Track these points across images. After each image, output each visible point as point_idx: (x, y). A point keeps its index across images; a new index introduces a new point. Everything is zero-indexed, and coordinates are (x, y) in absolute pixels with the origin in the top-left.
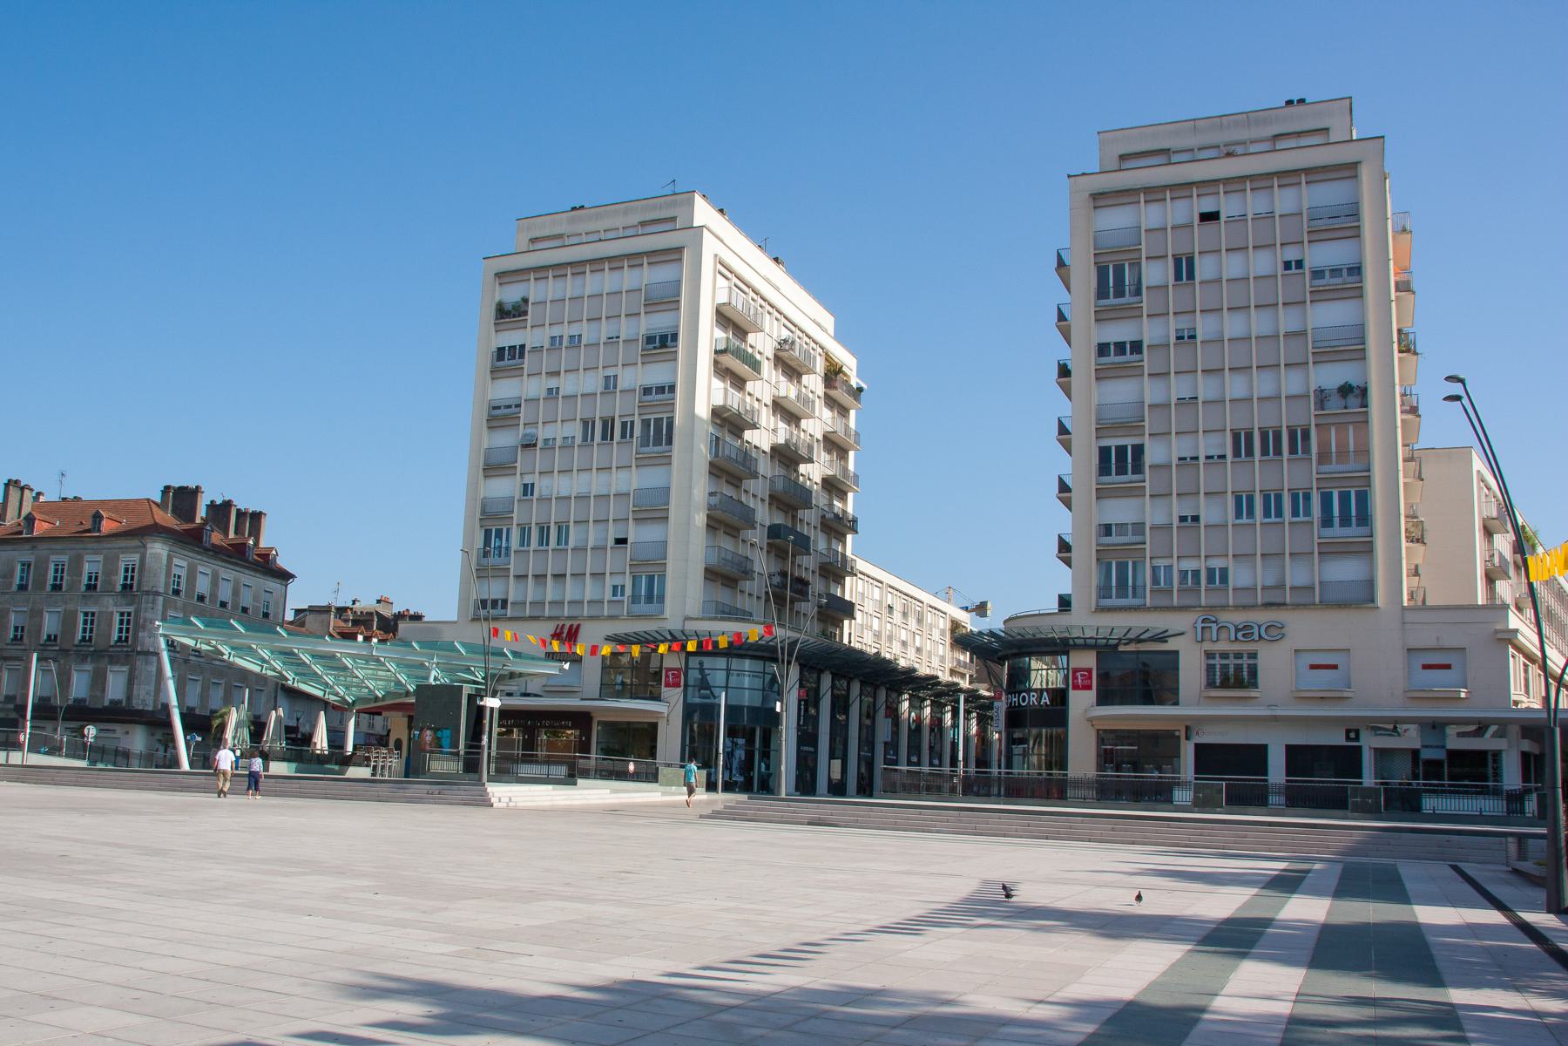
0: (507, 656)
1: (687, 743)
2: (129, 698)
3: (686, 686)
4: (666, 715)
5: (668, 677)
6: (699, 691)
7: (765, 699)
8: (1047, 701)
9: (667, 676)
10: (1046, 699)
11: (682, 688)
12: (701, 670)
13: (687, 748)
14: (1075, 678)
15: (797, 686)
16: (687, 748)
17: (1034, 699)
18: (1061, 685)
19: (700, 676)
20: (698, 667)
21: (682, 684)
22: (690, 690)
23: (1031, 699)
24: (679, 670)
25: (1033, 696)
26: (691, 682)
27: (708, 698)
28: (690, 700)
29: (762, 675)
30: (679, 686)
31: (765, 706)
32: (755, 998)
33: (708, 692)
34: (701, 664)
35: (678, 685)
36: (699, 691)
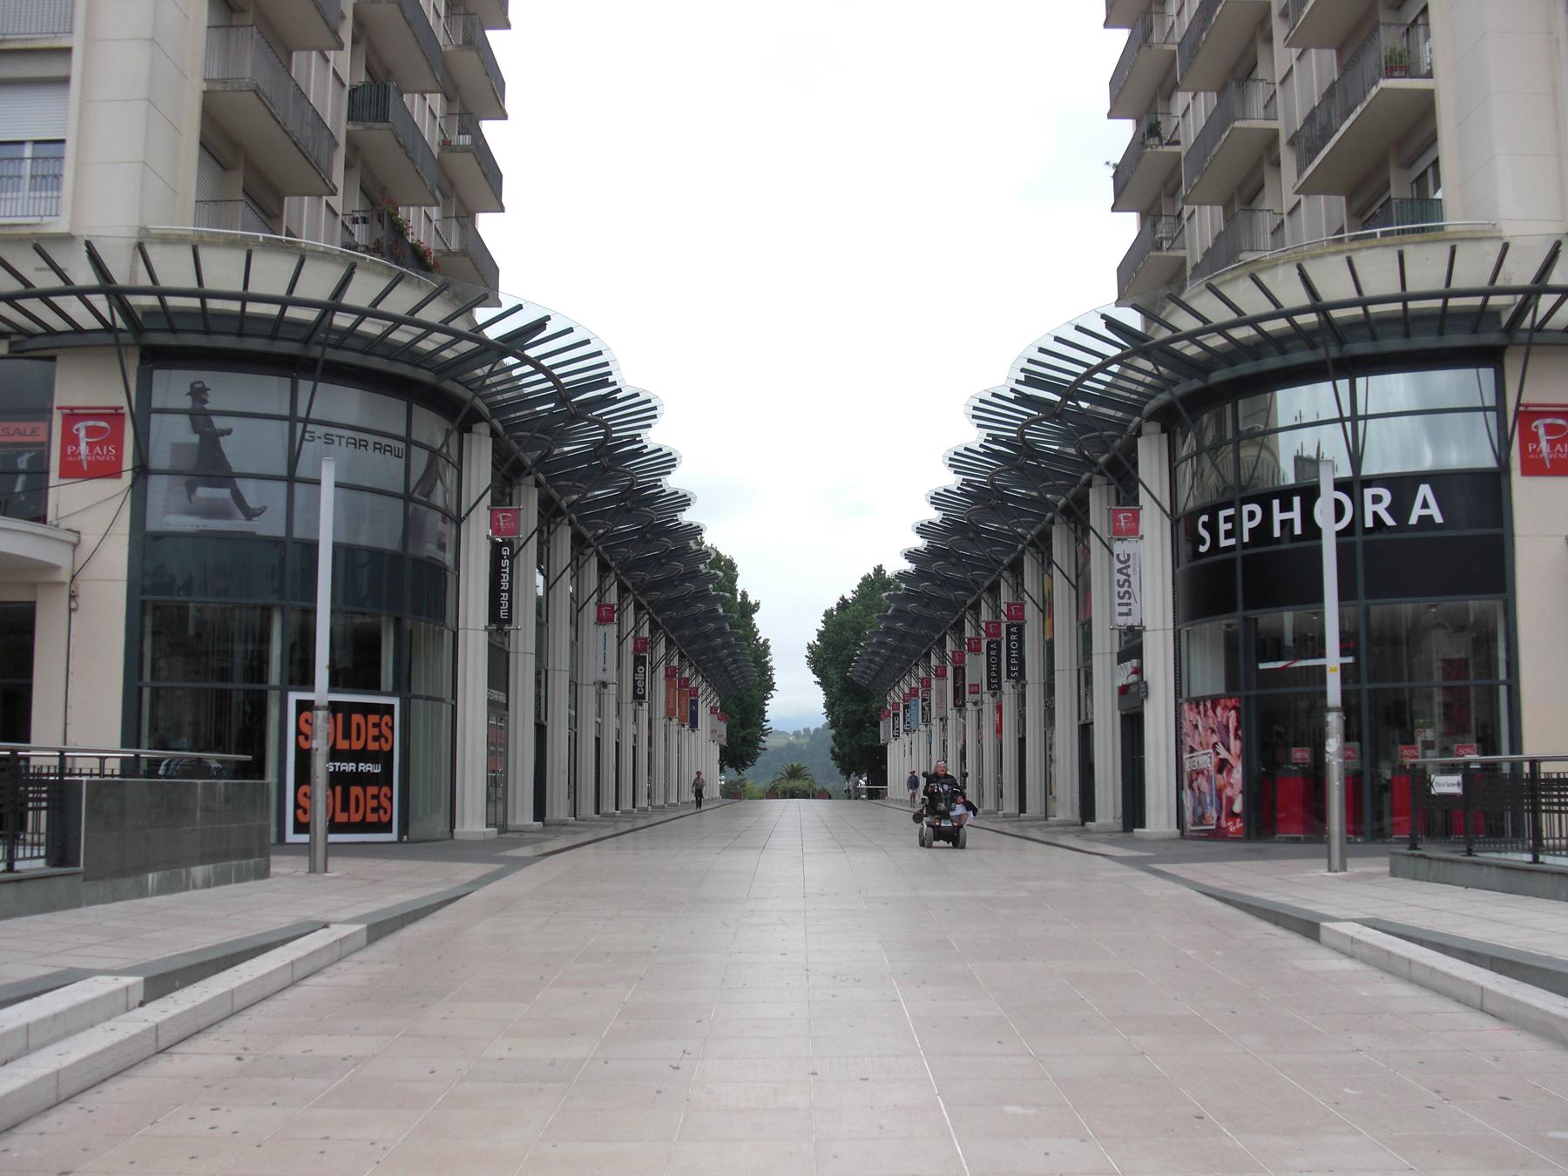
0: (1049, 1079)
1: (1503, 690)
2: (419, 697)
3: (142, 471)
4: (65, 576)
5: (75, 441)
6: (191, 489)
7: (411, 528)
8: (1434, 511)
9: (69, 439)
10: (1426, 505)
11: (127, 478)
12: (200, 416)
13: (1502, 675)
14: (1529, 437)
15: (487, 500)
16: (1502, 675)
17: (1381, 509)
18: (1488, 461)
19: (196, 439)
20: (187, 403)
21: (128, 462)
22: (158, 487)
23: (1369, 508)
24: (114, 416)
25: (1377, 499)
26: (160, 457)
27: (225, 514)
28: (154, 524)
29: (402, 445)
30: (117, 474)
31: (411, 551)
32: (27, 354)
33: (225, 493)
34: (198, 393)
35: (111, 471)
36: (191, 489)
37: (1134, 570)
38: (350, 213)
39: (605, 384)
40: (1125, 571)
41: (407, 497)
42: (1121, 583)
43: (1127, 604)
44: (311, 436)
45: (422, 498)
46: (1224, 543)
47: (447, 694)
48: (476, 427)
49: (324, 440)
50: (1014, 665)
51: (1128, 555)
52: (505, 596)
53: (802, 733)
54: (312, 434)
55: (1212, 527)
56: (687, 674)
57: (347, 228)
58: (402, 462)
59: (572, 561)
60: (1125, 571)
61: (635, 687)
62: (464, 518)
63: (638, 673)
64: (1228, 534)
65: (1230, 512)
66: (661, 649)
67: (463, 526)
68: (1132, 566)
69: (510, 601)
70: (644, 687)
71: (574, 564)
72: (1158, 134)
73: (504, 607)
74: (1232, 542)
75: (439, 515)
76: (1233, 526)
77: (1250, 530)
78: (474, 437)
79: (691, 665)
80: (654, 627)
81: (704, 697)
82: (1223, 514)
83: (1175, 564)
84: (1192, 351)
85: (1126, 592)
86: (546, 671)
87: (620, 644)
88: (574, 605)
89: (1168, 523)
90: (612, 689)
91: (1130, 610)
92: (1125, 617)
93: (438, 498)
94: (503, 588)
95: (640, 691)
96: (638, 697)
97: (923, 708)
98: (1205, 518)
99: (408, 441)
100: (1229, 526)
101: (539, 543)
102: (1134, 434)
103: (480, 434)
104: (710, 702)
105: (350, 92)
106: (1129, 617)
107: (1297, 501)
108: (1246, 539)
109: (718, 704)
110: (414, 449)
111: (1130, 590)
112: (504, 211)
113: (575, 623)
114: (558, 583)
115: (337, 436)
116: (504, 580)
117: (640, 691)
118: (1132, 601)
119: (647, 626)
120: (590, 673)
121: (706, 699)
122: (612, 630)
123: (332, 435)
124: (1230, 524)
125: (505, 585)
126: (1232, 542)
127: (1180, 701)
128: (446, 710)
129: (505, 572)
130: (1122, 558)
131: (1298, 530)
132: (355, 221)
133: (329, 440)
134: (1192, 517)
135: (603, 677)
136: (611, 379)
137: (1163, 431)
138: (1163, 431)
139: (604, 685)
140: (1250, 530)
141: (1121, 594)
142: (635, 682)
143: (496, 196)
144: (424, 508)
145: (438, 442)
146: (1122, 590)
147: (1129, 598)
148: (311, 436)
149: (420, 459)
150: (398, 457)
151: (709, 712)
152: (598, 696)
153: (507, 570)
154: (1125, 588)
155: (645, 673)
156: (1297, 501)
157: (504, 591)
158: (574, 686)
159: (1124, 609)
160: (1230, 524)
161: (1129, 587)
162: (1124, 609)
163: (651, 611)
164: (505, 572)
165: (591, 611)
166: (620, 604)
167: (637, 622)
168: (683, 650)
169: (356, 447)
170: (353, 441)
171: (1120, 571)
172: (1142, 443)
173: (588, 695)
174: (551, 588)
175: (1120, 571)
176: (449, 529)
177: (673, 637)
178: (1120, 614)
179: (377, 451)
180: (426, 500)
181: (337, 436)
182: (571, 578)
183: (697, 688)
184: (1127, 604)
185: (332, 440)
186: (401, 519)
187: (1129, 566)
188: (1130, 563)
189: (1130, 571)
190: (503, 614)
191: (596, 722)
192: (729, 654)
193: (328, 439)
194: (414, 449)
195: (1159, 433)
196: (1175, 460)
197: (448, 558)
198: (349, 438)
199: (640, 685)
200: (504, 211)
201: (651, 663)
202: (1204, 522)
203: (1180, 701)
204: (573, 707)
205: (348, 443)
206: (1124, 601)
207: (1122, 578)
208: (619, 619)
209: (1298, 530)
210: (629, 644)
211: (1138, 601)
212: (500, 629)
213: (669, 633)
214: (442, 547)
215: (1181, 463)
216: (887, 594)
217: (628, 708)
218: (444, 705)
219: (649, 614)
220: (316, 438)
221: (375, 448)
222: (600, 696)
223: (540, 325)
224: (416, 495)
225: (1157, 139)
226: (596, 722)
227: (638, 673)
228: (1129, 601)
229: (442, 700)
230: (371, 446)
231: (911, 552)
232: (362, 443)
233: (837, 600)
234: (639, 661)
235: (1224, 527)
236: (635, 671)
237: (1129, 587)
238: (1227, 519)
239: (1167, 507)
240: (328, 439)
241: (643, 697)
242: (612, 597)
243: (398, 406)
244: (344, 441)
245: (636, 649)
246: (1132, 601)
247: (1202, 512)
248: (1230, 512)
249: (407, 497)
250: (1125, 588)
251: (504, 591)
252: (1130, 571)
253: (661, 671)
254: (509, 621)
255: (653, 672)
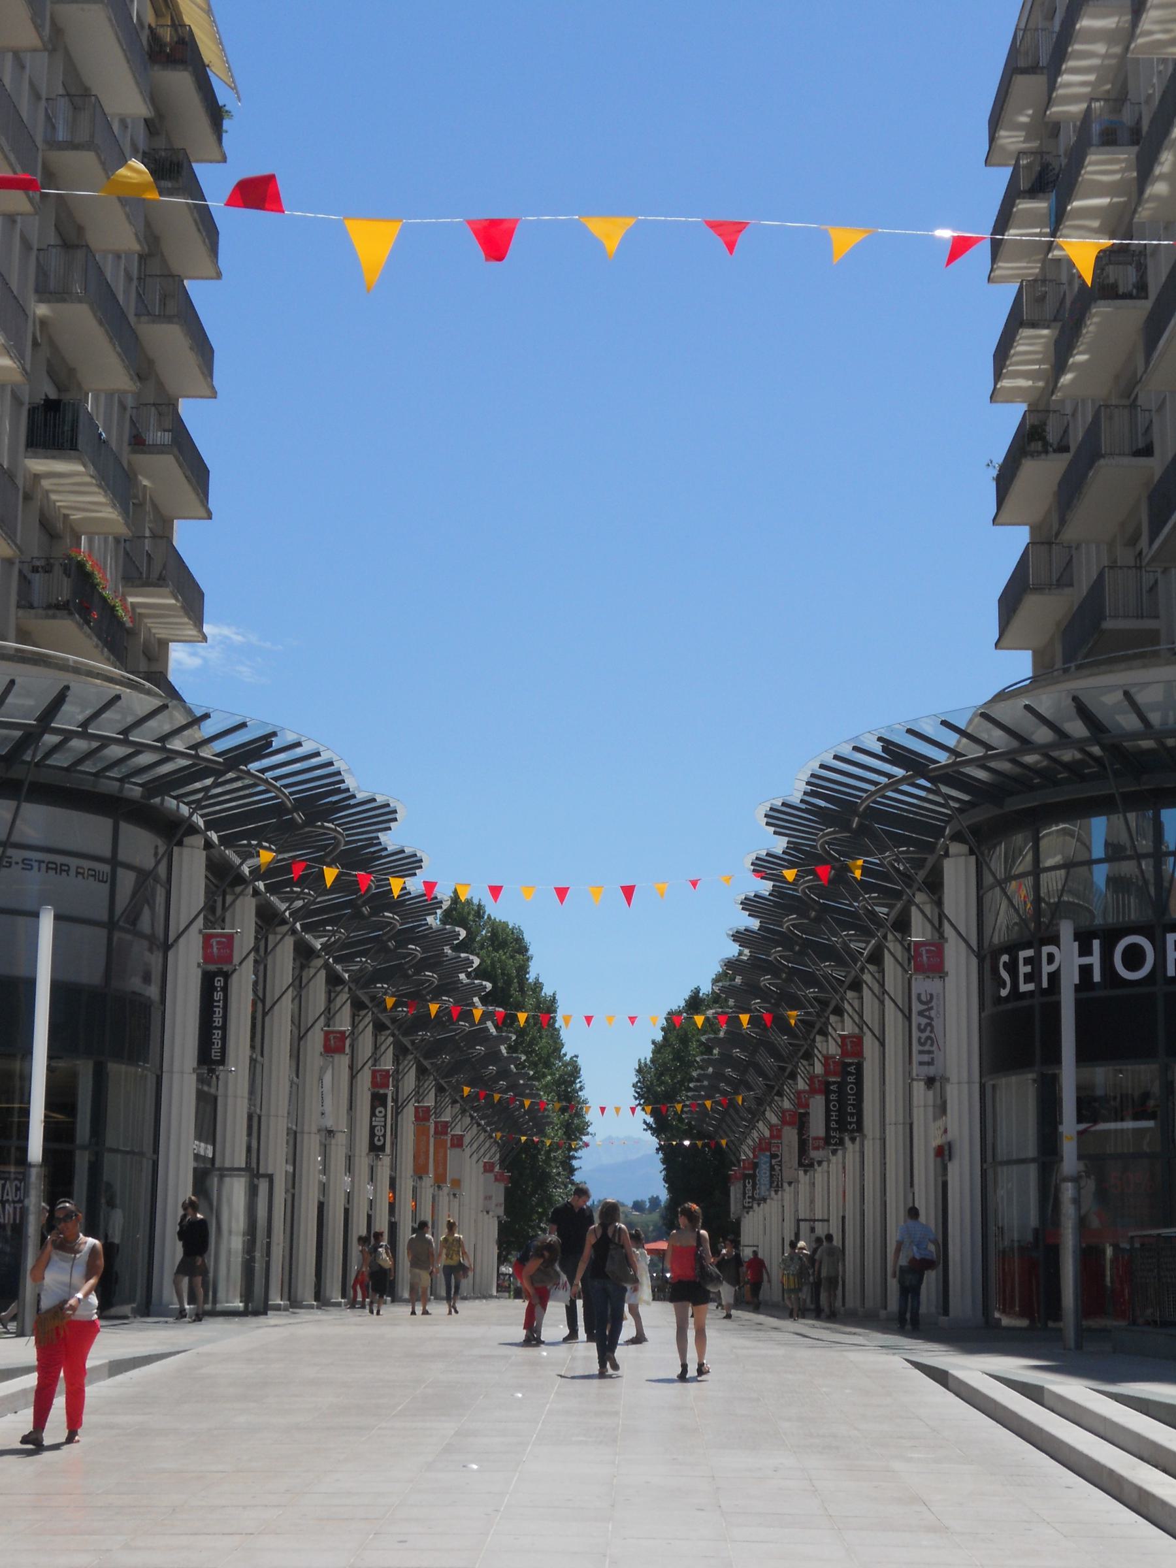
37: (938, 1012)
38: (29, 560)
39: (339, 791)
40: (927, 1013)
41: (111, 925)
42: (922, 1027)
43: (929, 1052)
44: (7, 862)
45: (128, 926)
46: (1024, 988)
47: (148, 1148)
48: (188, 840)
49: (21, 865)
50: (852, 1115)
51: (931, 995)
52: (218, 1033)
53: (648, 1205)
54: (10, 860)
55: (1012, 968)
56: (446, 1117)
57: (25, 577)
58: (106, 888)
59: (294, 981)
60: (927, 1013)
61: (372, 1134)
62: (172, 945)
63: (376, 1116)
64: (1029, 978)
65: (1029, 953)
66: (410, 1080)
67: (171, 954)
68: (935, 1008)
69: (224, 1039)
70: (384, 1136)
71: (297, 983)
72: (1043, 438)
73: (216, 1046)
74: (1031, 987)
75: (145, 943)
76: (1032, 968)
77: (1049, 974)
78: (186, 851)
79: (454, 1102)
80: (401, 1052)
81: (475, 1146)
82: (1024, 954)
83: (982, 1007)
84: (981, 775)
85: (929, 1038)
86: (260, 1117)
87: (353, 1077)
88: (296, 1032)
89: (974, 961)
90: (341, 1139)
91: (933, 1059)
92: (926, 1067)
93: (145, 924)
94: (216, 1024)
95: (379, 1140)
96: (375, 1149)
97: (772, 1168)
98: (1005, 958)
99: (114, 862)
100: (1028, 969)
101: (256, 961)
102: (942, 853)
103: (192, 847)
104: (484, 1155)
105: (29, 410)
106: (931, 1067)
107: (1096, 944)
108: (1045, 985)
109: (498, 1156)
110: (121, 872)
111: (933, 1035)
112: (211, 519)
113: (296, 1055)
114: (276, 1007)
115: (36, 861)
116: (217, 1015)
117: (379, 1140)
118: (934, 1048)
119: (390, 1053)
120: (312, 1123)
121: (479, 1148)
122: (343, 1061)
123: (31, 860)
124: (1030, 967)
125: (218, 1020)
126: (1031, 987)
127: (985, 1166)
128: (147, 1165)
129: (219, 1006)
130: (924, 998)
131: (1097, 977)
132: (35, 570)
133: (27, 864)
134: (996, 953)
135: (329, 1123)
136: (342, 786)
137: (972, 852)
138: (972, 852)
139: (330, 1133)
140: (1049, 974)
141: (922, 1040)
142: (372, 1128)
143: (202, 501)
144: (129, 937)
145: (148, 862)
146: (924, 1036)
147: (932, 1045)
148: (7, 862)
149: (127, 881)
150: (102, 881)
151: (482, 1170)
152: (323, 1148)
153: (221, 1004)
154: (927, 1033)
155: (385, 1116)
156: (1096, 944)
157: (217, 1028)
158: (294, 1137)
159: (926, 1058)
160: (1030, 967)
161: (932, 1031)
162: (926, 1058)
163: (397, 1032)
164: (219, 1006)
165: (316, 1039)
166: (354, 1026)
167: (376, 1047)
168: (442, 1082)
169: (56, 873)
170: (54, 866)
171: (921, 1013)
172: (948, 865)
173: (311, 1145)
174: (267, 1013)
175: (921, 1013)
176: (155, 959)
177: (426, 1063)
178: (921, 1063)
179: (80, 877)
180: (132, 928)
181: (36, 861)
182: (293, 1001)
183: (462, 1137)
184: (929, 1052)
185: (32, 866)
186: (103, 950)
187: (931, 1008)
188: (933, 1004)
189: (933, 1013)
190: (215, 1054)
191: (320, 1182)
192: (507, 1087)
193: (28, 865)
194: (121, 872)
195: (966, 855)
196: (982, 888)
197: (153, 991)
198: (49, 863)
199: (378, 1132)
200: (211, 519)
201: (395, 1100)
202: (1005, 962)
203: (985, 1166)
204: (291, 1161)
205: (48, 868)
206: (926, 1048)
207: (924, 1021)
208: (352, 1046)
209: (1097, 977)
210: (365, 1080)
211: (942, 1048)
212: (211, 1071)
213: (421, 1059)
214: (147, 979)
215: (988, 891)
216: (713, 1011)
217: (363, 1160)
218: (145, 1160)
219: (393, 1035)
220: (13, 864)
221: (78, 873)
222: (325, 1151)
223: (267, 739)
224: (121, 923)
225: (1040, 443)
226: (320, 1182)
227: (376, 1116)
228: (931, 1049)
229: (142, 1154)
230: (73, 872)
231: (732, 963)
232: (63, 868)
233: (687, 994)
234: (378, 1100)
235: (1024, 969)
236: (373, 1114)
237: (932, 1031)
238: (1028, 961)
239: (974, 943)
240: (28, 865)
241: (382, 1148)
242: (343, 1024)
243: (104, 824)
244: (43, 866)
245: (374, 1084)
246: (934, 1048)
247: (1028, 945)
248: (1029, 953)
249: (111, 925)
250: (927, 1033)
251: (217, 1028)
252: (933, 1013)
253: (409, 1113)
254: (222, 1061)
255: (398, 1111)
